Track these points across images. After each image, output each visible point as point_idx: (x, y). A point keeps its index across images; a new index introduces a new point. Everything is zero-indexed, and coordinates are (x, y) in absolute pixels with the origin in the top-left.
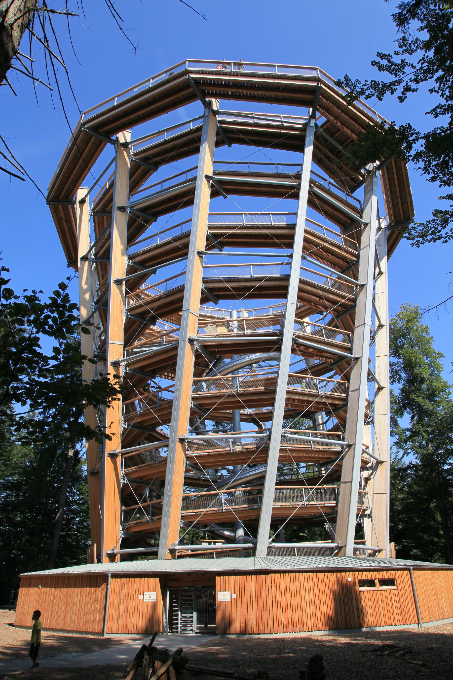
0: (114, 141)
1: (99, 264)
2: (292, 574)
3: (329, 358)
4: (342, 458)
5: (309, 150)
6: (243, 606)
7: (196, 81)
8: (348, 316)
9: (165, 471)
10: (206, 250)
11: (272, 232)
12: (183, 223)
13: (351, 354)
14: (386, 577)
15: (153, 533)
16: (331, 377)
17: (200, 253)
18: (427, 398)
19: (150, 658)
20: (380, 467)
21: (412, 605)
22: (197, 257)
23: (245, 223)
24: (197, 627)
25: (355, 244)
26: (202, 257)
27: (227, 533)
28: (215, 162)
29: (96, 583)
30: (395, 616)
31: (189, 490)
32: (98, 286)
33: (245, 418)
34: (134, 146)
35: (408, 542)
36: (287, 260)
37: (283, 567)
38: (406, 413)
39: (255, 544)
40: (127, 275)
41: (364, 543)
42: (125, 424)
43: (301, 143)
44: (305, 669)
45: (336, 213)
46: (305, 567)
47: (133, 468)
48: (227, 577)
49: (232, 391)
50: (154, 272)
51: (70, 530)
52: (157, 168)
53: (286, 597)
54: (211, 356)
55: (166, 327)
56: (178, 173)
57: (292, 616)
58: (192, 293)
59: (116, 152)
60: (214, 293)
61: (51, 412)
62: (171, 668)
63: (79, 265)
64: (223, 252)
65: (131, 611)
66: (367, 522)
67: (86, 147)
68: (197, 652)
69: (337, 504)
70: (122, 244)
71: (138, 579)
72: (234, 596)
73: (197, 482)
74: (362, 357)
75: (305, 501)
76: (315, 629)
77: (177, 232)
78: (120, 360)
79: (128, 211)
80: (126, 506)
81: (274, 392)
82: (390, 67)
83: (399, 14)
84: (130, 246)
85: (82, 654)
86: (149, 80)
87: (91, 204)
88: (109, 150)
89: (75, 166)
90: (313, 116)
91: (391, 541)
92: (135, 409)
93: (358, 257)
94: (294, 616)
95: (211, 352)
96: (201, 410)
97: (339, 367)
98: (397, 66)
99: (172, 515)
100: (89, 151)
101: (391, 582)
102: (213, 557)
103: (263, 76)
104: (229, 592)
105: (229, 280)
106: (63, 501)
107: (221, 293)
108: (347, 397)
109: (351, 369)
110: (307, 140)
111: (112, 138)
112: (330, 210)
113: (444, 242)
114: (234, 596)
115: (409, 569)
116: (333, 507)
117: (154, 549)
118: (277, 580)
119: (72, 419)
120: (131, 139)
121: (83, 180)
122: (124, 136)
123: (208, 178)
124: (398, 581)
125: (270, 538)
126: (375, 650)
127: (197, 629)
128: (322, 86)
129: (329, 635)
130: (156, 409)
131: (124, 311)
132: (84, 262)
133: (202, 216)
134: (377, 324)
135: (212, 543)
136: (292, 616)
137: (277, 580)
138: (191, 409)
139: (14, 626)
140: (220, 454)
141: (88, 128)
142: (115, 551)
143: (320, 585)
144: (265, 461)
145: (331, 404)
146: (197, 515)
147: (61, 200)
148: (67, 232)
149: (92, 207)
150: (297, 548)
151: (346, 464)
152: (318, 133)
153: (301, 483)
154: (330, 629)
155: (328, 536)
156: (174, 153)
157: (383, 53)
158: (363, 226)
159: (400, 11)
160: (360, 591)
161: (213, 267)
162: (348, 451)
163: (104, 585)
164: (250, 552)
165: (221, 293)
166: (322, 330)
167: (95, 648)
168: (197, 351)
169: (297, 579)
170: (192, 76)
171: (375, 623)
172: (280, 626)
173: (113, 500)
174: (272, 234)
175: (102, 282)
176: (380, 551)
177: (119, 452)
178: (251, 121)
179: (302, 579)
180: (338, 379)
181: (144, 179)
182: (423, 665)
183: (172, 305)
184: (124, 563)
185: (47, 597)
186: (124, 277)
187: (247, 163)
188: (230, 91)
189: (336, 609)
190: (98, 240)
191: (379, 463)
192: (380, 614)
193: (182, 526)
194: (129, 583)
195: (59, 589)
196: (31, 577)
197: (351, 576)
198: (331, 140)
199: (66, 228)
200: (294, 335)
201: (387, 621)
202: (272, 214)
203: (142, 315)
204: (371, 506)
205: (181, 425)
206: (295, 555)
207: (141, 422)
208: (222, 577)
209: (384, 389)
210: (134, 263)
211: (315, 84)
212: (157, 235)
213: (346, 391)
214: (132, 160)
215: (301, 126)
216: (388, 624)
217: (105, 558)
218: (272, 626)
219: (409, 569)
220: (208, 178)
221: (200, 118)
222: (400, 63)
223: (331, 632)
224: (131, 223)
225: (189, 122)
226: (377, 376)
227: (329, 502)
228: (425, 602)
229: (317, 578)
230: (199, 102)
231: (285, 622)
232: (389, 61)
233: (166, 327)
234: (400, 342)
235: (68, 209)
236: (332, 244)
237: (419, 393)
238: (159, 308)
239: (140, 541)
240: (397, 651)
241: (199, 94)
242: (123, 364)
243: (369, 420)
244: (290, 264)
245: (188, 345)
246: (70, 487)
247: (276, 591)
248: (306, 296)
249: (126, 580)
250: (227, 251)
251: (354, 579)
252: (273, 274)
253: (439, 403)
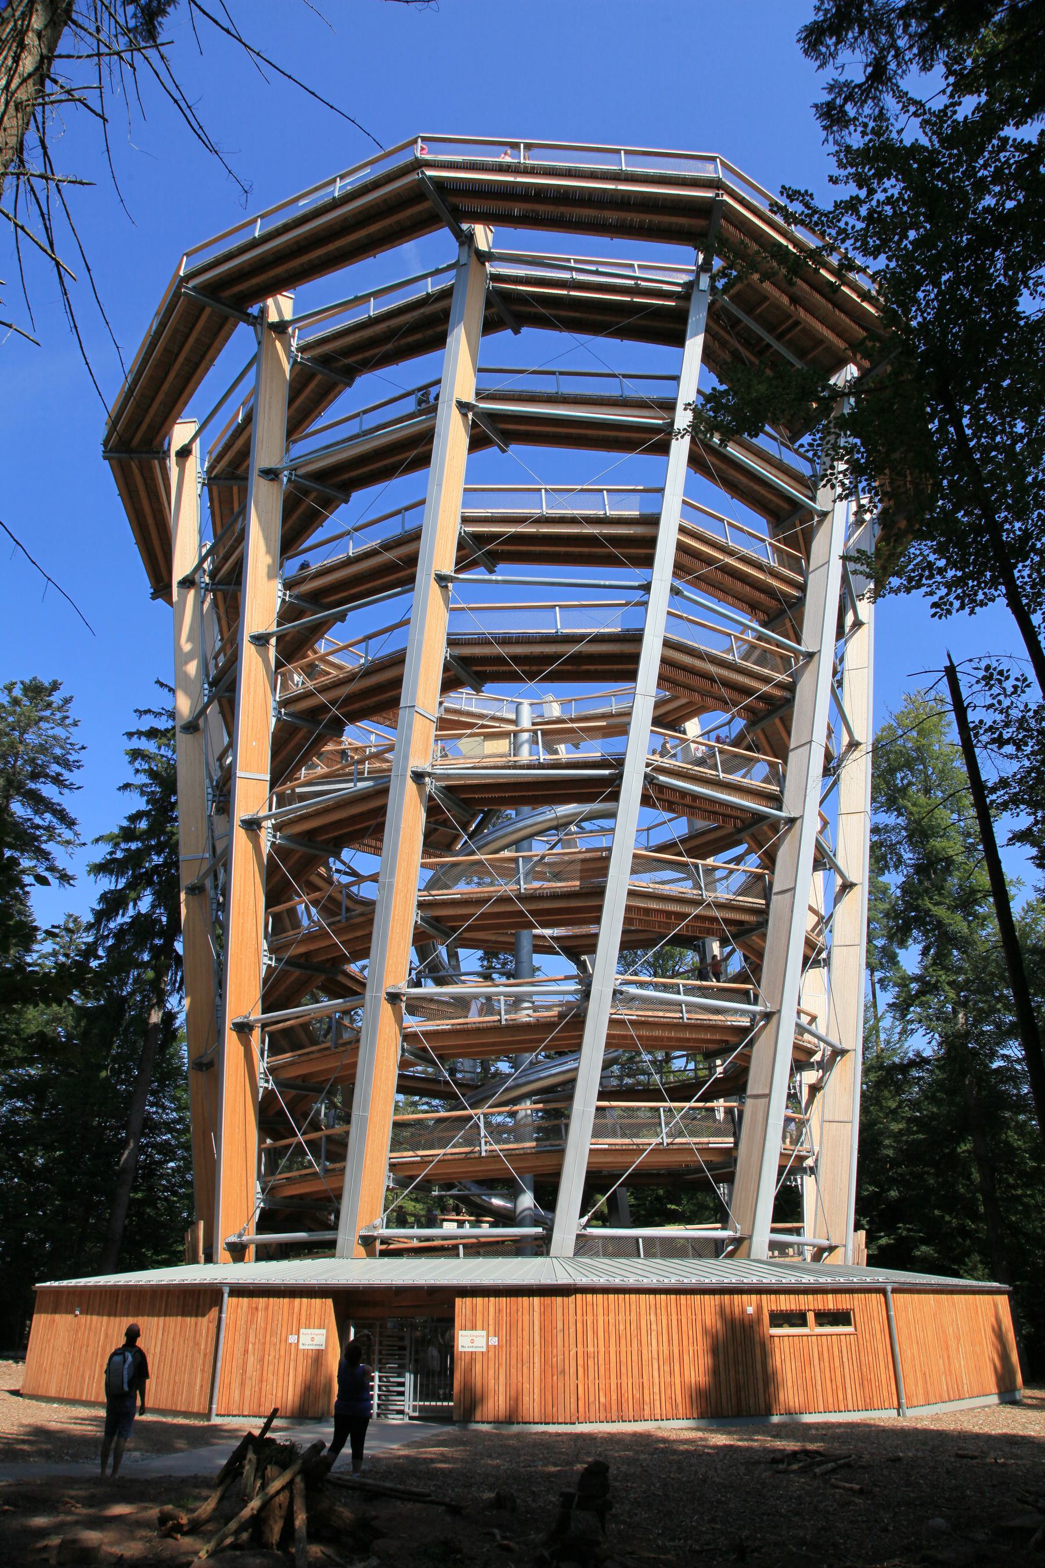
0: (255, 318)
1: (219, 595)
2: (621, 1296)
3: (730, 816)
4: (751, 1043)
5: (695, 345)
6: (514, 1362)
7: (440, 184)
8: (777, 721)
9: (354, 1065)
10: (456, 571)
11: (607, 530)
12: (407, 509)
13: (780, 809)
14: (831, 1307)
15: (329, 1199)
16: (738, 860)
17: (441, 579)
18: (956, 907)
19: (258, 1459)
20: (840, 1064)
21: (887, 1367)
22: (434, 587)
23: (546, 511)
24: (414, 1406)
25: (799, 559)
26: (446, 587)
27: (497, 1202)
28: (480, 370)
29: (198, 1306)
30: (849, 1391)
31: (427, 1103)
32: (218, 645)
33: (542, 948)
34: (299, 329)
35: (909, 1230)
36: (637, 596)
37: (602, 1281)
38: (910, 941)
39: (550, 1230)
40: (279, 625)
41: (798, 1231)
42: (271, 959)
43: (679, 327)
44: (571, 1490)
45: (757, 487)
46: (651, 1280)
47: (286, 1057)
48: (479, 1300)
49: (506, 887)
50: (342, 617)
51: (151, 1188)
52: (352, 380)
53: (607, 1345)
54: (463, 810)
55: (373, 737)
56: (397, 394)
57: (619, 1387)
58: (422, 670)
59: (259, 343)
60: (468, 668)
61: (112, 925)
62: (298, 1479)
63: (175, 598)
64: (494, 578)
65: (271, 1368)
66: (808, 1186)
67: (191, 329)
68: (400, 1457)
69: (736, 1144)
70: (268, 552)
71: (286, 1300)
72: (494, 1341)
73: (436, 1087)
74: (802, 817)
75: (667, 1134)
76: (670, 1416)
77: (393, 529)
78: (261, 814)
79: (285, 479)
80: (274, 1139)
81: (599, 892)
82: (810, 216)
83: (828, 104)
84: (288, 558)
85: (154, 1455)
86: (334, 181)
87: (202, 460)
88: (241, 339)
89: (167, 374)
90: (706, 267)
91: (857, 1227)
92: (296, 924)
93: (803, 588)
94: (624, 1385)
95: (464, 800)
96: (437, 927)
97: (754, 837)
98: (826, 215)
99: (368, 1162)
100: (197, 340)
101: (841, 1318)
102: (458, 1255)
103: (593, 175)
104: (484, 1333)
105: (506, 640)
106: (136, 1124)
107: (488, 669)
108: (768, 905)
109: (781, 840)
110: (692, 320)
111: (250, 311)
112: (744, 480)
113: (927, 594)
114: (494, 1341)
115: (882, 1291)
116: (728, 1151)
117: (327, 1236)
118: (589, 1308)
119: (158, 942)
120: (294, 314)
121: (186, 403)
122: (281, 306)
123: (463, 407)
124: (858, 1317)
125: (582, 1216)
126: (775, 1461)
127: (414, 1411)
128: (726, 198)
129: (698, 1429)
130: (340, 925)
131: (272, 704)
132: (184, 591)
133: (449, 493)
134: (845, 740)
135: (467, 1225)
136: (619, 1387)
137: (589, 1308)
138: (416, 928)
139: (21, 1395)
140: (478, 1030)
141: (194, 289)
142: (244, 1238)
143: (684, 1321)
144: (576, 1048)
145: (727, 921)
146: (424, 1162)
147: (135, 451)
148: (150, 521)
149: (206, 465)
150: (644, 1238)
151: (759, 1053)
152: (718, 305)
153: (653, 1094)
154: (701, 1416)
155: (720, 1215)
156: (389, 346)
157: (794, 188)
158: (816, 519)
159: (829, 98)
160: (772, 1336)
161: (471, 609)
162: (764, 1026)
163: (214, 1312)
164: (540, 1247)
165: (488, 669)
166: (714, 755)
167: (180, 1444)
168: (431, 798)
169: (633, 1307)
170: (430, 173)
171: (802, 1405)
172: (592, 1407)
173: (242, 1126)
175: (226, 636)
176: (831, 1249)
177: (257, 1021)
178: (565, 275)
179: (643, 1306)
180: (752, 863)
181: (324, 404)
182: (861, 1491)
183: (378, 693)
184: (263, 1264)
185: (92, 1335)
186: (274, 628)
187: (553, 373)
188: (517, 209)
189: (715, 1372)
190: (218, 539)
191: (839, 1053)
192: (814, 1386)
193: (391, 1185)
194: (267, 1308)
195: (118, 1319)
196: (58, 1291)
197: (754, 1303)
198: (747, 321)
199: (147, 510)
200: (648, 765)
201: (830, 1401)
202: (608, 491)
203: (314, 714)
204: (816, 1149)
205: (393, 961)
206: (639, 1256)
207: (307, 955)
208: (468, 1300)
209: (855, 888)
210: (297, 597)
211: (710, 194)
212: (348, 533)
213: (767, 893)
214: (295, 361)
215: (679, 289)
216: (831, 1407)
217: (222, 1252)
218: (573, 1406)
219: (882, 1291)
220: (463, 406)
221: (450, 268)
222: (832, 209)
223: (703, 1423)
224: (290, 505)
225: (424, 277)
226: (840, 862)
227: (720, 1139)
228: (917, 1362)
229: (678, 1305)
231: (602, 1400)
232: (807, 206)
233: (373, 737)
234: (902, 779)
235: (151, 470)
236: (744, 559)
237: (940, 894)
238: (351, 698)
239: (301, 1217)
240: (820, 1464)
241: (446, 215)
242: (268, 824)
243: (815, 956)
244: (645, 603)
245: (411, 786)
246: (154, 1093)
247: (585, 1333)
248: (680, 676)
249: (262, 1301)
250: (505, 572)
251: (759, 1308)
252: (607, 626)
253: (985, 919)
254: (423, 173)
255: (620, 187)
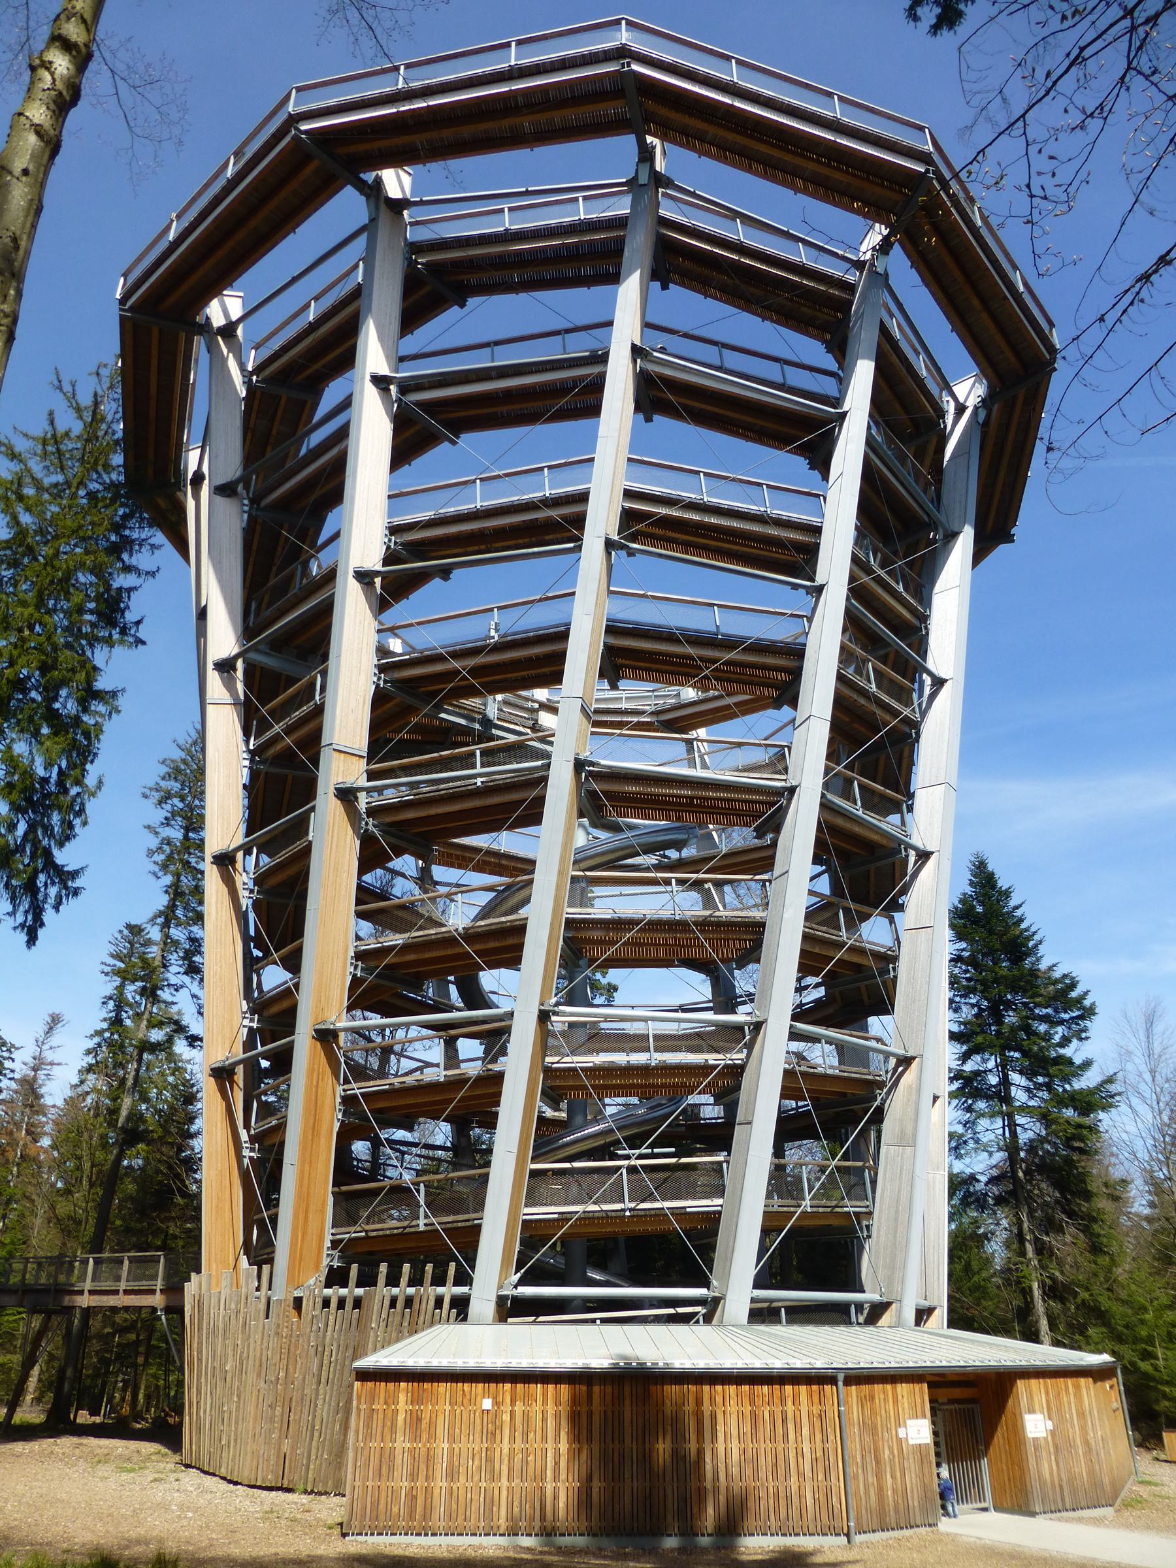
122: (224, 308)
146: (564, 1218)
174: (564, 517)
230: (631, 139)
254: (297, 129)
255: (431, 103)
